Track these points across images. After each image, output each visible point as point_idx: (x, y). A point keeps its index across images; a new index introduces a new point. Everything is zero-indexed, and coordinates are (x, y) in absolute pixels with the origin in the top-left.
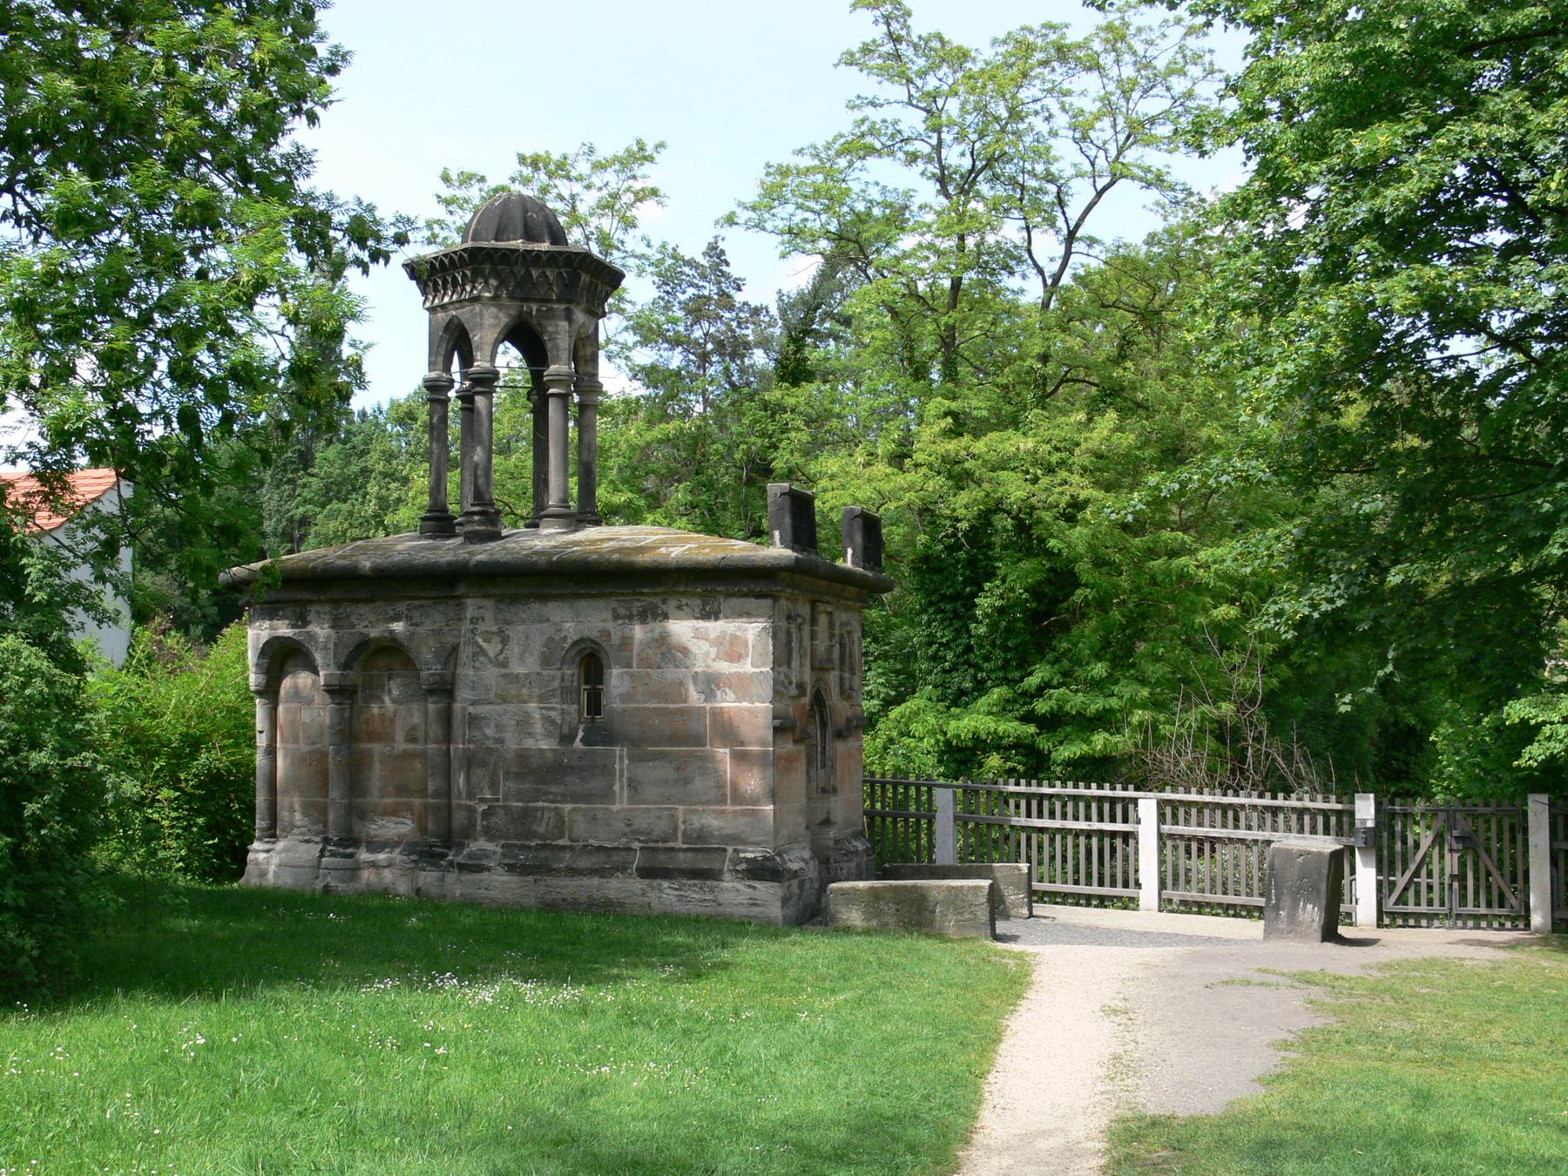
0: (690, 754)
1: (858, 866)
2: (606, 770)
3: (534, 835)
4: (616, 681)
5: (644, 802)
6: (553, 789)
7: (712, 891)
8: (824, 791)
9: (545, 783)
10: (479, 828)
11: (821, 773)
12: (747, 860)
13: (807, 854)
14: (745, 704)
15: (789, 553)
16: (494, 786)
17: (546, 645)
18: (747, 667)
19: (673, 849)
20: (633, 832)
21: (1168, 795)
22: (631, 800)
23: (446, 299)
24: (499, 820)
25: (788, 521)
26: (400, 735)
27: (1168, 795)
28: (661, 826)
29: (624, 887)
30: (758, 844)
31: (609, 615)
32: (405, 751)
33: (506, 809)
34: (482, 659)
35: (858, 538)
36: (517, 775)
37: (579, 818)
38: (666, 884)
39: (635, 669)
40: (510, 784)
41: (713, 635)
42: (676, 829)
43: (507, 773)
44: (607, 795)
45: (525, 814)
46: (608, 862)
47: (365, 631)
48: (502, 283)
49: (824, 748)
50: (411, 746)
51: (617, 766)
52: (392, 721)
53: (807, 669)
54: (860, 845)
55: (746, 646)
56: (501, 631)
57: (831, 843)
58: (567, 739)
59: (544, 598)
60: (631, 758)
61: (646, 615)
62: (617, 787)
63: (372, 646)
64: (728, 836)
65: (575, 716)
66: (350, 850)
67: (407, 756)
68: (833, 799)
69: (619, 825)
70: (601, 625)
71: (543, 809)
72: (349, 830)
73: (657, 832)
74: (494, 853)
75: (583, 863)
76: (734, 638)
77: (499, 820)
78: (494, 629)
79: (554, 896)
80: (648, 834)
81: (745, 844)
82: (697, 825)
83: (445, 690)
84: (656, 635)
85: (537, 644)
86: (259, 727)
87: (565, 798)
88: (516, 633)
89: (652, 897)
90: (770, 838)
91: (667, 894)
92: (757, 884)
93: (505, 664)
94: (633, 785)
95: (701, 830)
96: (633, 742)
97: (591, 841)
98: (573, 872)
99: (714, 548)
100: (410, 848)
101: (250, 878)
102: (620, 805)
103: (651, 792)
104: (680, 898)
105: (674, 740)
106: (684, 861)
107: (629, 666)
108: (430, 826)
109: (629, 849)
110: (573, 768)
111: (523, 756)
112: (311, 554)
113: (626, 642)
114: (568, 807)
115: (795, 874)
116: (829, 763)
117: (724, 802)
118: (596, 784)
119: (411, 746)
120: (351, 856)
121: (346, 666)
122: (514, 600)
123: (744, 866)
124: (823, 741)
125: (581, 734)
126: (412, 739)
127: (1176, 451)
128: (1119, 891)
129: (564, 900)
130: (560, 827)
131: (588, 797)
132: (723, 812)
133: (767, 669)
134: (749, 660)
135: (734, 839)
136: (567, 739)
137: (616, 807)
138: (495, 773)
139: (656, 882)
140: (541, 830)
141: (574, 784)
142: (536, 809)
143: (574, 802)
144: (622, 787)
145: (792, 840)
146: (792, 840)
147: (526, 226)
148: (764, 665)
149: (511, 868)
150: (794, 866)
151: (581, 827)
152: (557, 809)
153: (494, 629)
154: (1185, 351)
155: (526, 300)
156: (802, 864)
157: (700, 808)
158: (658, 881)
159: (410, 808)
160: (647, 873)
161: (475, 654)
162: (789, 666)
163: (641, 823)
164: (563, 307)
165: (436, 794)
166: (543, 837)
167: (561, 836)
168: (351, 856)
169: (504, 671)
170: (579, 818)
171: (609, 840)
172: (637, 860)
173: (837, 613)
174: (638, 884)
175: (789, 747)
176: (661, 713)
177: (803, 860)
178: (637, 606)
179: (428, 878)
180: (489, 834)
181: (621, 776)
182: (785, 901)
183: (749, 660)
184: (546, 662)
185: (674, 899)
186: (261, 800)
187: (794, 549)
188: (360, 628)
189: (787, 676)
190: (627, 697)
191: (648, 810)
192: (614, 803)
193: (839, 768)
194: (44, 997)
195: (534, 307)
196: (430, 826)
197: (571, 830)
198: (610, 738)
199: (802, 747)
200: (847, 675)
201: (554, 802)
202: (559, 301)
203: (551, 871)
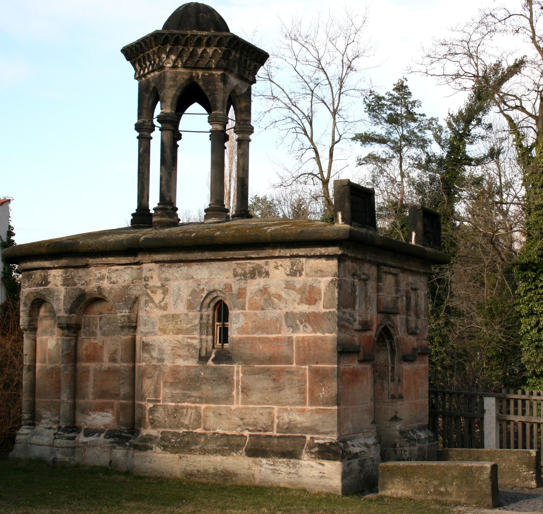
0: (282, 370)
1: (420, 449)
3: (183, 425)
5: (252, 403)
6: (194, 394)
7: (294, 466)
8: (393, 397)
9: (189, 389)
10: (147, 420)
11: (392, 385)
12: (319, 445)
13: (371, 441)
14: (319, 334)
15: (348, 226)
16: (156, 392)
17: (191, 295)
18: (320, 308)
19: (270, 436)
20: (245, 424)
22: (244, 402)
23: (146, 71)
25: (347, 205)
26: (106, 357)
28: (263, 420)
30: (326, 433)
31: (230, 274)
32: (109, 368)
33: (165, 407)
34: (151, 304)
35: (420, 225)
36: (172, 384)
37: (210, 414)
38: (264, 461)
39: (247, 311)
40: (167, 390)
41: (298, 286)
42: (273, 422)
43: (165, 383)
45: (176, 410)
47: (82, 287)
48: (180, 56)
49: (393, 368)
50: (112, 365)
51: (235, 378)
52: (102, 347)
53: (375, 312)
54: (423, 435)
55: (320, 294)
56: (163, 286)
57: (397, 433)
60: (244, 373)
62: (234, 393)
63: (88, 298)
64: (306, 427)
65: (210, 343)
66: (72, 435)
67: (109, 371)
68: (399, 403)
70: (226, 281)
71: (187, 407)
72: (73, 420)
73: (261, 424)
74: (156, 437)
76: (312, 287)
78: (159, 284)
79: (192, 468)
80: (255, 425)
81: (319, 433)
82: (287, 420)
84: (261, 287)
86: (25, 352)
87: (208, 400)
89: (256, 469)
90: (335, 429)
92: (326, 463)
93: (165, 308)
95: (289, 423)
96: (246, 361)
97: (218, 431)
100: (111, 434)
104: (274, 471)
105: (272, 360)
107: (243, 308)
108: (121, 419)
109: (242, 436)
110: (207, 379)
111: (175, 371)
113: (241, 293)
114: (203, 406)
115: (356, 455)
116: (396, 378)
117: (304, 404)
119: (112, 365)
120: (73, 438)
123: (316, 449)
124: (393, 363)
125: (213, 356)
126: (113, 360)
129: (198, 471)
130: (199, 419)
132: (303, 411)
133: (334, 310)
134: (322, 303)
136: (203, 359)
137: (233, 407)
138: (157, 383)
139: (258, 460)
140: (186, 422)
141: (206, 389)
142: (183, 408)
143: (207, 402)
144: (238, 393)
145: (357, 431)
146: (357, 431)
147: (198, 21)
148: (332, 307)
150: (357, 450)
151: (211, 421)
152: (196, 407)
153: (159, 284)
155: (196, 68)
156: (364, 449)
157: (289, 407)
158: (260, 458)
159: (111, 406)
161: (146, 302)
162: (354, 308)
163: (249, 419)
164: (219, 73)
165: (125, 397)
166: (187, 427)
167: (199, 427)
168: (73, 438)
169: (165, 313)
170: (210, 414)
171: (229, 429)
173: (401, 276)
175: (355, 365)
177: (366, 445)
178: (249, 265)
179: (119, 453)
181: (238, 385)
182: (344, 475)
183: (322, 303)
185: (269, 472)
186: (25, 399)
187: (351, 224)
188: (79, 286)
189: (352, 316)
190: (242, 330)
191: (255, 409)
192: (232, 403)
193: (404, 381)
195: (200, 73)
196: (121, 419)
197: (205, 422)
199: (368, 366)
200: (412, 318)
201: (194, 403)
202: (217, 68)
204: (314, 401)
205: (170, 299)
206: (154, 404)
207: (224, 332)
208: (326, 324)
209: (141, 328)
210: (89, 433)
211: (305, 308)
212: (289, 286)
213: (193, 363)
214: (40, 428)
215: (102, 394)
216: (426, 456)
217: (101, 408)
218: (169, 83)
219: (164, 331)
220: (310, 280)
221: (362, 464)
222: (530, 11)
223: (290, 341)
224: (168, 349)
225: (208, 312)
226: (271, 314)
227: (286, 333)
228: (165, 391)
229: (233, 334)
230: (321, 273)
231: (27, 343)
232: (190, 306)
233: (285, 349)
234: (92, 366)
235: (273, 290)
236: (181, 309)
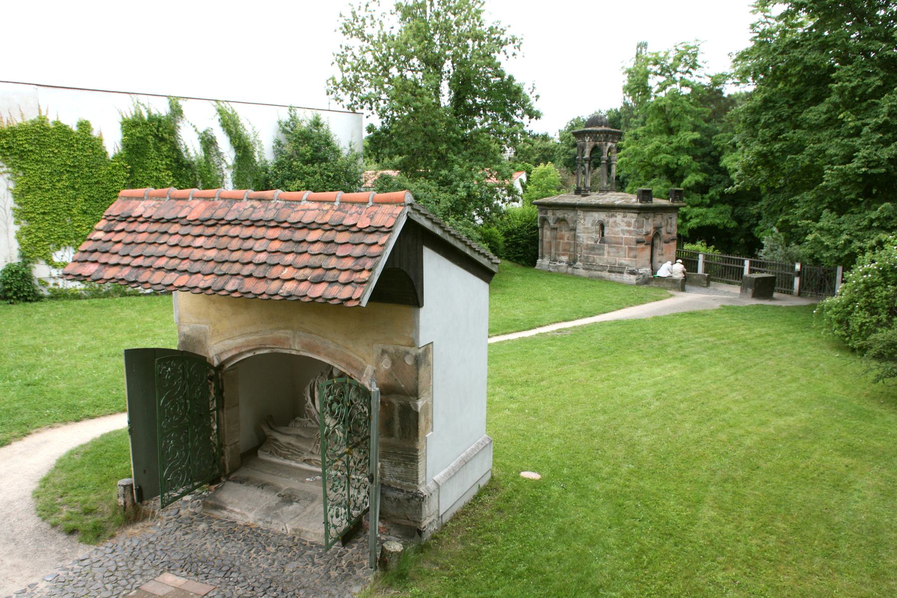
2: (603, 249)
4: (606, 231)
16: (581, 251)
18: (632, 228)
21: (752, 259)
24: (582, 258)
26: (566, 238)
27: (752, 259)
28: (613, 262)
29: (606, 274)
44: (603, 254)
45: (587, 257)
46: (603, 268)
59: (592, 211)
61: (612, 216)
67: (567, 243)
69: (605, 261)
75: (598, 268)
77: (582, 258)
83: (574, 229)
85: (591, 221)
87: (597, 255)
91: (613, 276)
94: (608, 253)
96: (609, 243)
98: (595, 270)
102: (606, 256)
103: (612, 254)
105: (617, 243)
106: (617, 270)
111: (587, 245)
113: (608, 222)
118: (601, 252)
122: (587, 211)
127: (401, 574)
128: (789, 290)
130: (594, 261)
131: (600, 255)
135: (627, 265)
136: (596, 242)
141: (597, 252)
149: (584, 269)
151: (598, 261)
160: (610, 271)
163: (609, 261)
172: (608, 269)
176: (615, 237)
178: (611, 214)
180: (580, 261)
190: (608, 234)
194: (64, 246)
198: (604, 242)
203: (591, 270)
204: (629, 257)
205: (586, 222)
206: (649, 204)
207: (603, 235)
208: (633, 234)
209: (577, 231)
210: (560, 262)
211: (627, 228)
212: (623, 221)
213: (593, 243)
214: (545, 260)
215: (565, 250)
216: (535, 248)
217: (564, 255)
218: (587, 147)
219: (584, 232)
220: (629, 220)
221: (644, 276)
222: (327, 496)
223: (622, 238)
224: (585, 237)
225: (598, 227)
226: (617, 229)
227: (621, 235)
228: (584, 251)
229: (605, 235)
230: (632, 217)
231: (540, 231)
232: (592, 225)
233: (621, 241)
234: (561, 241)
235: (618, 222)
236: (589, 225)
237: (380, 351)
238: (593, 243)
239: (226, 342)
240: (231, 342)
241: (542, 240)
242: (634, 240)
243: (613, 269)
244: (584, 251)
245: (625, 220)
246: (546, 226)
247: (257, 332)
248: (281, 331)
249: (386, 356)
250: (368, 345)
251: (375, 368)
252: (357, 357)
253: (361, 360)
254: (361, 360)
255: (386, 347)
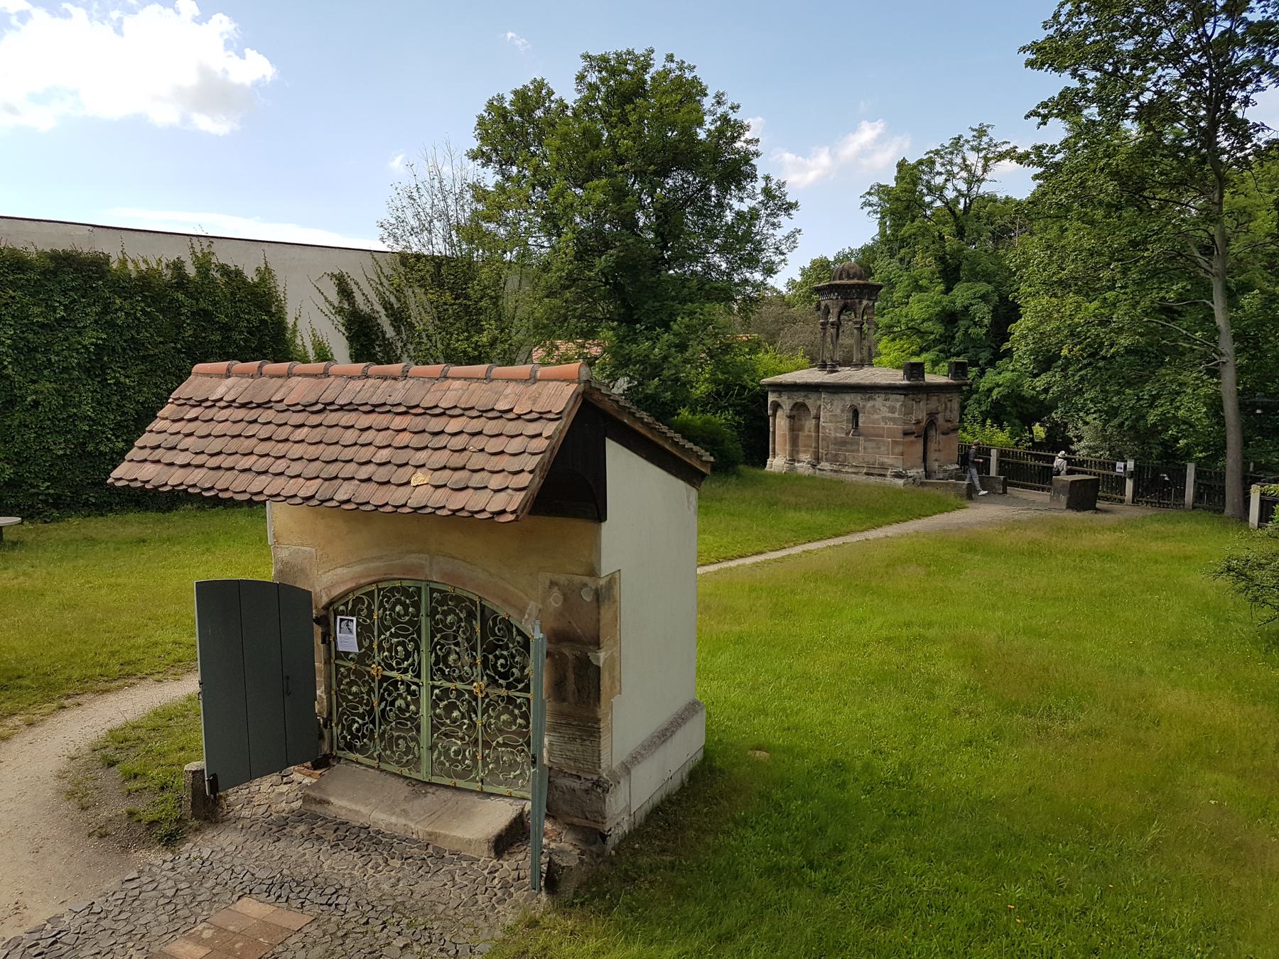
2: (858, 444)
18: (896, 415)
28: (872, 461)
44: (858, 451)
51: (644, 415)
58: (847, 434)
77: (829, 456)
88: (835, 403)
98: (847, 473)
99: (536, 660)
101: (767, 468)
103: (870, 450)
106: (876, 471)
111: (836, 438)
112: (813, 429)
113: (864, 407)
118: (854, 448)
121: (791, 410)
131: (852, 451)
135: (892, 466)
136: (847, 434)
141: (849, 447)
154: (1270, 181)
174: (865, 477)
180: (827, 460)
184: (842, 411)
190: (863, 423)
212: (884, 405)
225: (851, 415)
226: (876, 416)
227: (883, 424)
228: (831, 447)
236: (839, 411)
237: (548, 583)
238: (843, 435)
239: (339, 571)
240: (345, 570)
241: (774, 432)
242: (901, 432)
243: (872, 471)
244: (831, 447)
245: (888, 403)
246: (779, 413)
247: (381, 558)
248: (413, 555)
249: (556, 589)
250: (531, 575)
251: (541, 606)
252: (516, 591)
253: (521, 594)
254: (521, 594)
255: (556, 577)
